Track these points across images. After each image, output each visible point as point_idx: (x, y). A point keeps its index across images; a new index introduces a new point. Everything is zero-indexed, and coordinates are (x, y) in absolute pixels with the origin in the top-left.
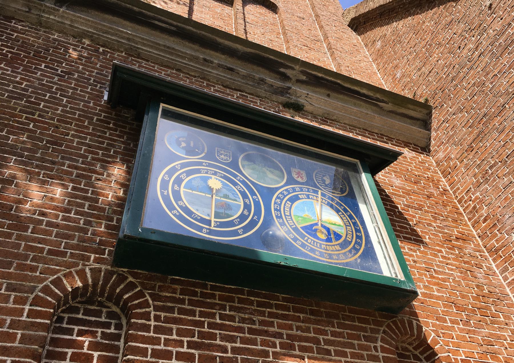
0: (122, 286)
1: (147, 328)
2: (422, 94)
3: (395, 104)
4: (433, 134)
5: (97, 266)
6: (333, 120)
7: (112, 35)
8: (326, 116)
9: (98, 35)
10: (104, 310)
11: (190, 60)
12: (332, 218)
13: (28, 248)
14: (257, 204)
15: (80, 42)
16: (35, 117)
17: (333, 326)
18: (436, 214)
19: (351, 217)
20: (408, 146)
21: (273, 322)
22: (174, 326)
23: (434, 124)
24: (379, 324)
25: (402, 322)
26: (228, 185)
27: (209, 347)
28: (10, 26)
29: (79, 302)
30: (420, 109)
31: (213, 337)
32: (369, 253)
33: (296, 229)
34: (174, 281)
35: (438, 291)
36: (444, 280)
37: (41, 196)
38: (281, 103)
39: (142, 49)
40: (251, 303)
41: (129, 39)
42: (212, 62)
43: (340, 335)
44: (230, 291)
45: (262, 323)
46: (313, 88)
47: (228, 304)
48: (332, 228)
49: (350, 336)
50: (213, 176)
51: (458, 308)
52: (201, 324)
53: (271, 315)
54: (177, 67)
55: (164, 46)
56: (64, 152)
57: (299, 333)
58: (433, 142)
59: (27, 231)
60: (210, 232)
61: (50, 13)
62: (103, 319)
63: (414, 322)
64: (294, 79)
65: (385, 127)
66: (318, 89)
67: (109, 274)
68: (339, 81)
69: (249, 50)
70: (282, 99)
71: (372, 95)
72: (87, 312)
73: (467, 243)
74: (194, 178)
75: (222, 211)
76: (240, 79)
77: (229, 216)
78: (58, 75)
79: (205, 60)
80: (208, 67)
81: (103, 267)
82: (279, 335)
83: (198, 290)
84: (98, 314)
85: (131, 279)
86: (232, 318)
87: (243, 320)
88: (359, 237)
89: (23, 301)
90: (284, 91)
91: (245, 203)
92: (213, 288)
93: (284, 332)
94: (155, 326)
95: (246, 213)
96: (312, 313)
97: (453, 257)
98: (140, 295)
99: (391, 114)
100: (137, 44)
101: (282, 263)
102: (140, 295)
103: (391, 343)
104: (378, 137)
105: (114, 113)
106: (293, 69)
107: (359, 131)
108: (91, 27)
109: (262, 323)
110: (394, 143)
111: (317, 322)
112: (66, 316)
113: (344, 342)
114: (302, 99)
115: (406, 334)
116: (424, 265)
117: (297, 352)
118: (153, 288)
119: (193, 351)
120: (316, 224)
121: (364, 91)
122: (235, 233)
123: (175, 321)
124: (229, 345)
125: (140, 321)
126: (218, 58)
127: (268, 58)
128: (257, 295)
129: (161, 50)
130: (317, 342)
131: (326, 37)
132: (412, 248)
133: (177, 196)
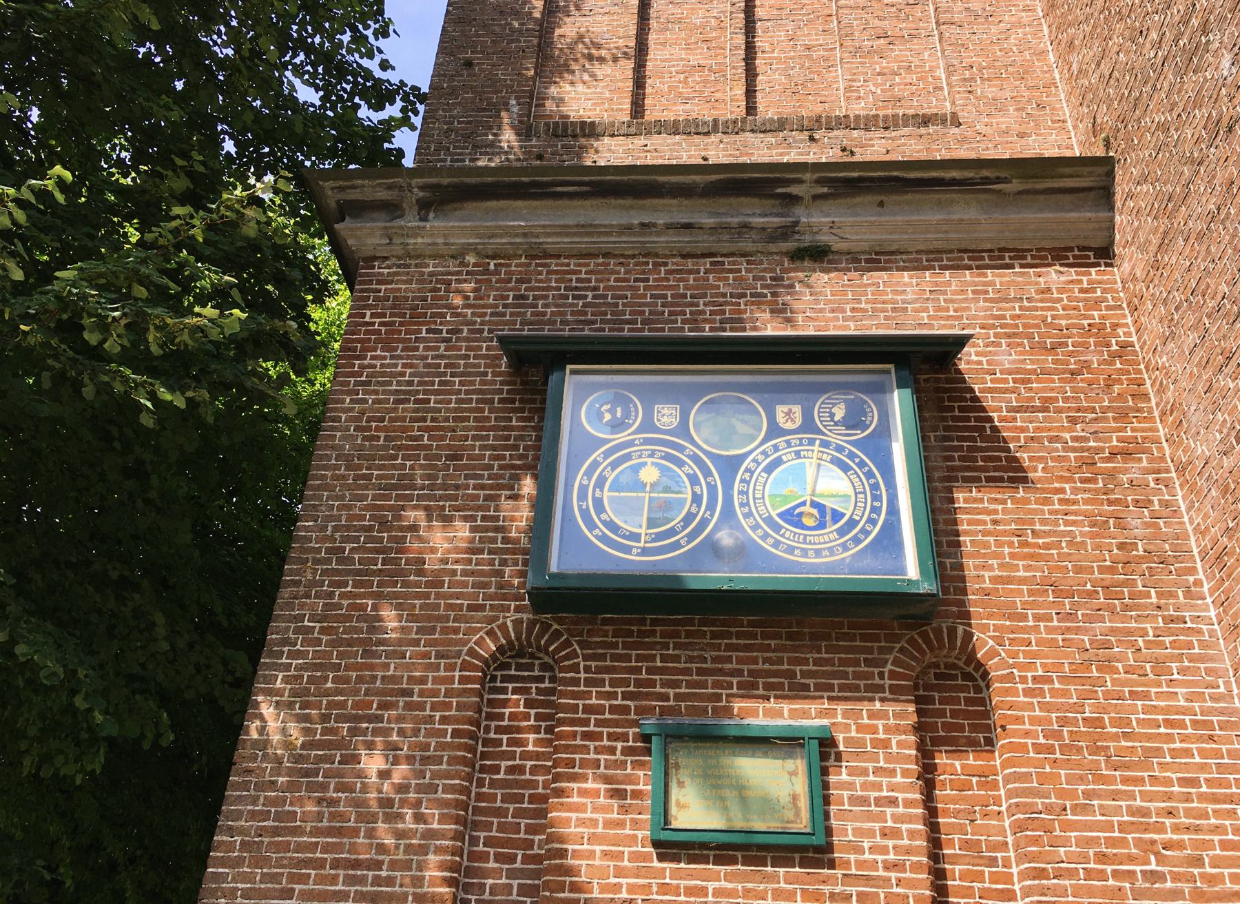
0: (547, 637)
1: (576, 682)
2: (1073, 143)
3: (1024, 177)
4: (1118, 218)
5: (519, 616)
6: (892, 253)
7: (501, 236)
8: (878, 249)
9: (483, 244)
10: (537, 662)
11: (620, 234)
13: (450, 607)
14: (712, 489)
15: (462, 264)
16: (428, 423)
17: (819, 652)
18: (1079, 410)
21: (731, 657)
22: (606, 676)
23: (1120, 191)
24: (895, 638)
25: (938, 632)
26: (669, 469)
27: (648, 696)
28: (374, 275)
29: (509, 657)
30: (1089, 169)
31: (652, 684)
33: (769, 521)
35: (1027, 568)
36: (1047, 546)
37: (444, 542)
38: (786, 254)
39: (547, 243)
40: (704, 635)
41: (525, 235)
42: (654, 225)
44: (676, 623)
46: (848, 200)
47: (671, 641)
48: (830, 504)
49: (843, 662)
50: (649, 460)
51: (1058, 593)
52: (638, 670)
53: (729, 648)
54: (603, 251)
55: (577, 226)
56: (466, 467)
57: (766, 666)
59: (443, 587)
60: (644, 551)
62: (536, 673)
63: (960, 629)
64: (807, 197)
65: (1007, 234)
66: (858, 200)
67: (532, 623)
68: (895, 174)
69: (714, 177)
71: (971, 175)
72: (519, 667)
73: (1133, 459)
74: (622, 472)
75: (659, 515)
76: (706, 237)
77: (669, 521)
78: (444, 340)
79: (643, 225)
80: (651, 234)
81: (525, 616)
82: (739, 673)
83: (635, 628)
84: (530, 667)
85: (556, 626)
86: (676, 659)
87: (691, 659)
89: (450, 668)
90: (786, 232)
91: (694, 493)
93: (745, 667)
94: (585, 679)
95: (694, 510)
96: (790, 637)
97: (1086, 496)
98: (567, 644)
99: (1025, 197)
100: (537, 237)
101: (725, 588)
102: (567, 644)
103: (908, 664)
104: (991, 258)
105: (519, 380)
107: (948, 259)
108: (471, 236)
110: (1029, 260)
111: (795, 649)
112: (499, 673)
113: (833, 672)
114: (824, 234)
115: (941, 646)
116: (1013, 527)
117: (761, 692)
118: (581, 634)
119: (628, 703)
120: (804, 504)
122: (676, 545)
123: (608, 670)
124: (671, 692)
125: (568, 675)
126: (662, 213)
127: (750, 179)
128: (713, 623)
129: (575, 234)
132: (999, 496)
133: (599, 505)
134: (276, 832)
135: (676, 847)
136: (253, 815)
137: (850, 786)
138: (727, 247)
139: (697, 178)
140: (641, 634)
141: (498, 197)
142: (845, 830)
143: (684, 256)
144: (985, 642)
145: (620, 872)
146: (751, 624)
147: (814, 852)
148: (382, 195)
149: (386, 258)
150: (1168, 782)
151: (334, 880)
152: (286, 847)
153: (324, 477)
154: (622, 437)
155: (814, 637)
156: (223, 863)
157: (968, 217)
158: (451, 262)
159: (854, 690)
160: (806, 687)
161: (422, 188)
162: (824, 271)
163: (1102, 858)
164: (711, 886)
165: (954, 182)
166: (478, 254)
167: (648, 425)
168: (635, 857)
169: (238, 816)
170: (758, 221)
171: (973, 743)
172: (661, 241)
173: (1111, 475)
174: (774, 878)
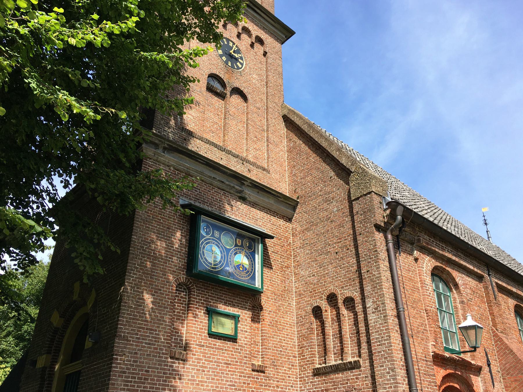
12: (245, 261)
14: (225, 256)
15: (170, 169)
19: (252, 261)
20: (283, 218)
23: (297, 210)
24: (250, 298)
32: (253, 278)
34: (201, 282)
36: (274, 284)
40: (218, 289)
43: (239, 301)
45: (220, 296)
48: (245, 265)
49: (241, 301)
51: (275, 294)
53: (223, 294)
58: (294, 218)
61: (161, 157)
70: (239, 195)
82: (224, 300)
87: (216, 295)
88: (252, 270)
90: (241, 192)
92: (209, 284)
96: (233, 293)
106: (247, 181)
109: (220, 296)
121: (274, 193)
130: (233, 302)
131: (267, 131)
134: (133, 319)
135: (212, 335)
136: (128, 314)
137: (240, 327)
138: (228, 190)
139: (228, 171)
140: (207, 286)
141: (183, 155)
142: (239, 336)
143: (219, 188)
144: (263, 302)
145: (202, 339)
146: (227, 289)
147: (233, 339)
148: (157, 142)
149: (151, 159)
150: (285, 334)
151: (147, 333)
152: (136, 323)
153: (138, 224)
154: (208, 237)
155: (237, 295)
156: (122, 325)
157: (270, 201)
158: (167, 167)
159: (243, 308)
160: (235, 305)
161: (168, 145)
162: (245, 204)
163: (275, 347)
164: (217, 344)
165: (273, 194)
166: (174, 168)
167: (213, 235)
168: (205, 336)
169: (124, 314)
170: (237, 187)
171: (257, 322)
172: (216, 183)
173: (285, 271)
174: (227, 344)
